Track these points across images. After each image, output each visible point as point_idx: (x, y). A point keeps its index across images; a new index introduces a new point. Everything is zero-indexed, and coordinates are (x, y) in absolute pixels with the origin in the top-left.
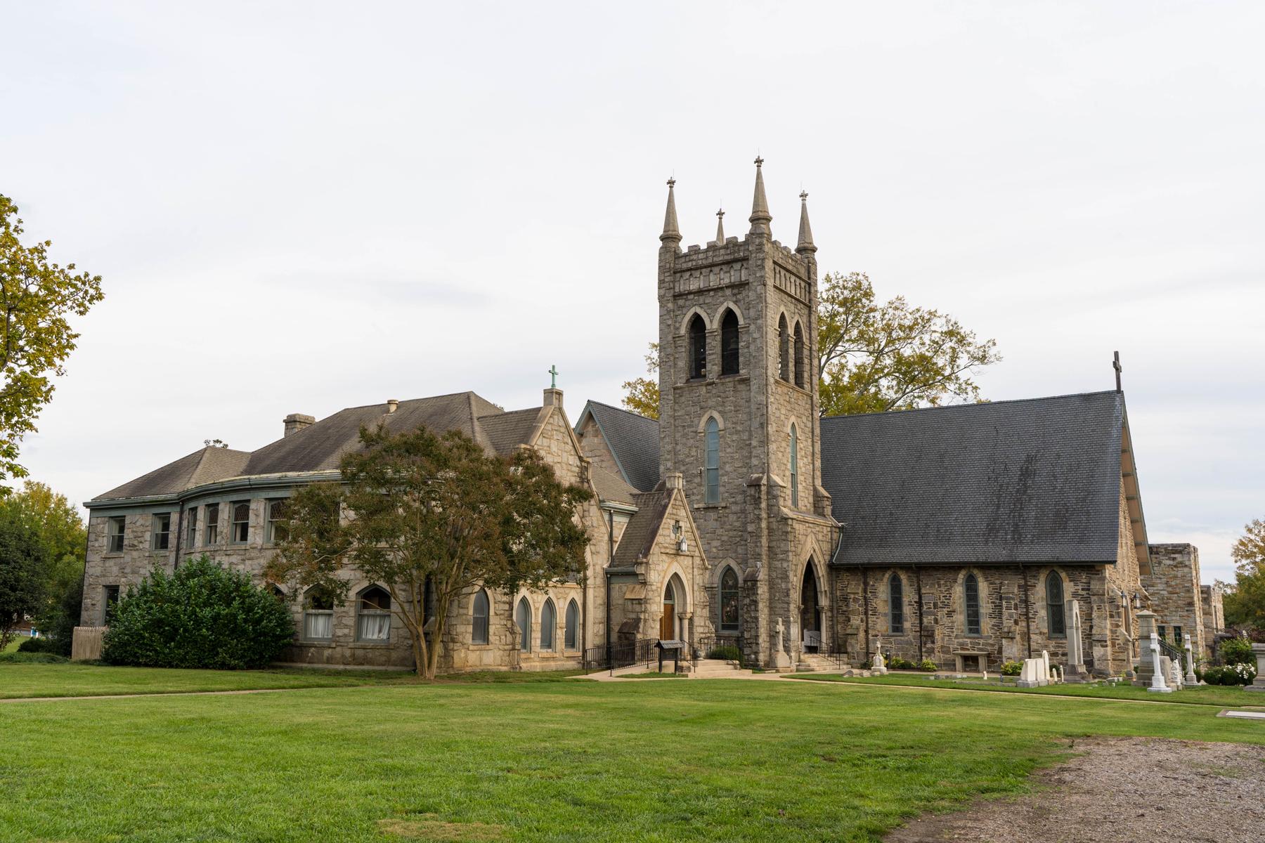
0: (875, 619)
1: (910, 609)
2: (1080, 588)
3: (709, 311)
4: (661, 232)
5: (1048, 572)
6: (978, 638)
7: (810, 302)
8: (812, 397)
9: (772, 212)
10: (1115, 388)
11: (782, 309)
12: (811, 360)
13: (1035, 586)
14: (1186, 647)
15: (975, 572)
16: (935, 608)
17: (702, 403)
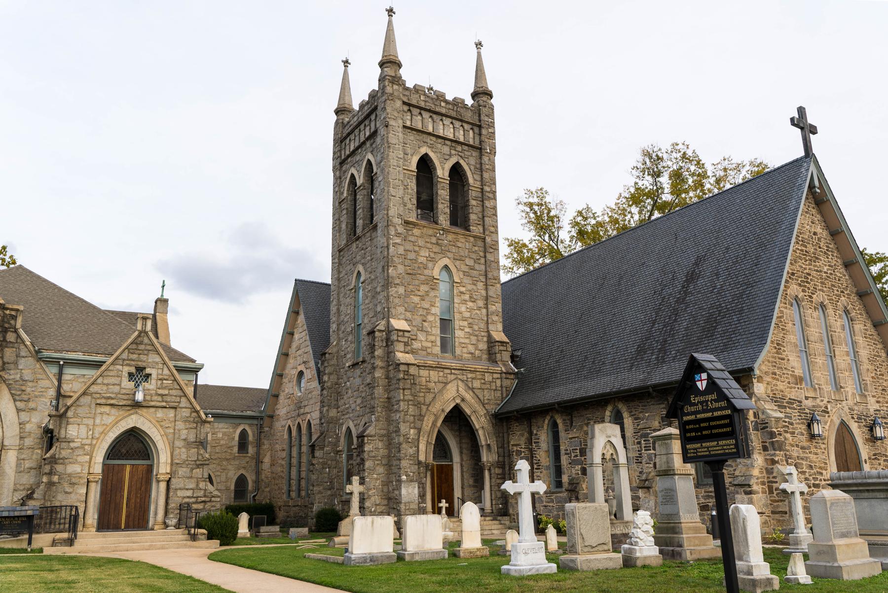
0: (539, 474)
4: (335, 106)
8: (484, 239)
9: (401, 58)
10: (801, 153)
11: (424, 150)
12: (483, 201)
15: (621, 406)
16: (581, 456)
17: (363, 261)
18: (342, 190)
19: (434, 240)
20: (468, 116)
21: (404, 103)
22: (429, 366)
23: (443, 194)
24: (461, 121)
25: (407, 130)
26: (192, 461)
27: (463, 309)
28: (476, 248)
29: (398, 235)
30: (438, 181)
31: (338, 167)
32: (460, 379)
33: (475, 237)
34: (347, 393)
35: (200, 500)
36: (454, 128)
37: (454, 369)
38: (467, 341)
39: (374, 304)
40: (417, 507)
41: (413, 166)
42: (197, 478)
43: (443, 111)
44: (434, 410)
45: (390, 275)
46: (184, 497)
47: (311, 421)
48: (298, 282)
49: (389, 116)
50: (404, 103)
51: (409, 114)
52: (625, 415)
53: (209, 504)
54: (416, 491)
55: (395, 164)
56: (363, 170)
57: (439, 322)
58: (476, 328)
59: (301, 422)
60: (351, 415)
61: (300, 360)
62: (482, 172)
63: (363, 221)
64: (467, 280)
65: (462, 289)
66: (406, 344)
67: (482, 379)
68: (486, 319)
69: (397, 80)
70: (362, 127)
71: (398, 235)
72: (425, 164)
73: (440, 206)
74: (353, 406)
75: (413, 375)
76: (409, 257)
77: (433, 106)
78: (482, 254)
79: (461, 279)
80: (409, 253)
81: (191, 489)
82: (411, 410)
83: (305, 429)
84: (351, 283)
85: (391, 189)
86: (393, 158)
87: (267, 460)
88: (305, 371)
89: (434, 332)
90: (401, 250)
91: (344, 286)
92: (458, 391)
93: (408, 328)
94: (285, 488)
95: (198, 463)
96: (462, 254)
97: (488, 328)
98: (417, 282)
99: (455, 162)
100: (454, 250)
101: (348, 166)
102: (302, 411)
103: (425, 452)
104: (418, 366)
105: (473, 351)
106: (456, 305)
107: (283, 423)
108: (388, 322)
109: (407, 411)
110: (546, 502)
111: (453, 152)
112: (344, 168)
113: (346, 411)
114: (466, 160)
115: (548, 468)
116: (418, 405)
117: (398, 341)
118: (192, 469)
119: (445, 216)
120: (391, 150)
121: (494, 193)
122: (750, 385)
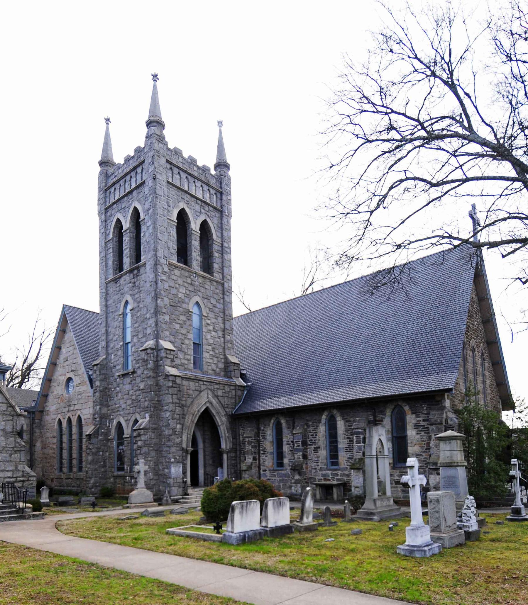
0: (264, 457)
1: (288, 448)
2: (421, 419)
3: (124, 214)
4: (99, 159)
5: (393, 406)
6: (336, 470)
7: (221, 207)
8: (223, 284)
9: (164, 118)
11: (182, 205)
12: (222, 254)
13: (382, 421)
14: (512, 473)
15: (335, 412)
16: (302, 446)
18: (108, 232)
19: (189, 281)
20: (213, 182)
21: (168, 161)
22: (189, 378)
23: (195, 243)
24: (208, 185)
25: (169, 185)
26: (10, 448)
27: (209, 337)
28: (218, 291)
29: (164, 273)
30: (192, 233)
31: (103, 211)
32: (209, 389)
33: (217, 282)
34: (117, 396)
35: (18, 479)
36: (203, 190)
37: (205, 381)
38: (211, 361)
39: (143, 328)
40: (181, 481)
41: (174, 218)
42: (16, 462)
43: (196, 174)
44: (192, 411)
45: (159, 305)
46: (5, 478)
47: (81, 416)
48: (65, 307)
49: (157, 170)
50: (168, 161)
51: (170, 171)
52: (339, 418)
53: (27, 482)
54: (181, 469)
55: (162, 213)
56: (129, 216)
57: (192, 345)
58: (217, 351)
59: (71, 417)
60: (122, 413)
61: (68, 369)
62: (222, 230)
63: (130, 259)
64: (211, 315)
65: (209, 322)
66: (172, 360)
67: (223, 389)
68: (223, 345)
69: (161, 139)
70: (128, 178)
71: (164, 273)
72: (182, 216)
73: (194, 254)
74: (124, 406)
75: (179, 384)
76: (171, 293)
77: (188, 168)
78: (221, 296)
79: (207, 313)
80: (172, 289)
81: (11, 471)
82: (177, 410)
83: (75, 421)
84: (119, 310)
85: (159, 234)
86: (160, 208)
87: (38, 444)
88: (73, 377)
89: (189, 353)
90: (166, 286)
91: (112, 312)
92: (208, 397)
93: (173, 348)
94: (57, 466)
95: (15, 449)
96: (209, 294)
97: (224, 352)
98: (177, 313)
99: (204, 219)
100: (202, 290)
101: (113, 211)
102: (72, 408)
103: (185, 440)
104: (182, 378)
105: (215, 369)
106: (204, 333)
107: (54, 417)
108: (157, 342)
109: (175, 411)
110: (270, 477)
111: (203, 211)
112: (109, 214)
113: (117, 410)
114: (211, 219)
115: (272, 453)
116: (182, 406)
117: (166, 357)
118: (11, 455)
119: (196, 262)
120: (158, 200)
121: (230, 248)
122: (443, 401)
